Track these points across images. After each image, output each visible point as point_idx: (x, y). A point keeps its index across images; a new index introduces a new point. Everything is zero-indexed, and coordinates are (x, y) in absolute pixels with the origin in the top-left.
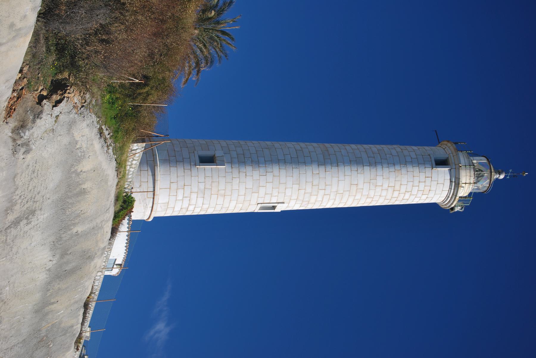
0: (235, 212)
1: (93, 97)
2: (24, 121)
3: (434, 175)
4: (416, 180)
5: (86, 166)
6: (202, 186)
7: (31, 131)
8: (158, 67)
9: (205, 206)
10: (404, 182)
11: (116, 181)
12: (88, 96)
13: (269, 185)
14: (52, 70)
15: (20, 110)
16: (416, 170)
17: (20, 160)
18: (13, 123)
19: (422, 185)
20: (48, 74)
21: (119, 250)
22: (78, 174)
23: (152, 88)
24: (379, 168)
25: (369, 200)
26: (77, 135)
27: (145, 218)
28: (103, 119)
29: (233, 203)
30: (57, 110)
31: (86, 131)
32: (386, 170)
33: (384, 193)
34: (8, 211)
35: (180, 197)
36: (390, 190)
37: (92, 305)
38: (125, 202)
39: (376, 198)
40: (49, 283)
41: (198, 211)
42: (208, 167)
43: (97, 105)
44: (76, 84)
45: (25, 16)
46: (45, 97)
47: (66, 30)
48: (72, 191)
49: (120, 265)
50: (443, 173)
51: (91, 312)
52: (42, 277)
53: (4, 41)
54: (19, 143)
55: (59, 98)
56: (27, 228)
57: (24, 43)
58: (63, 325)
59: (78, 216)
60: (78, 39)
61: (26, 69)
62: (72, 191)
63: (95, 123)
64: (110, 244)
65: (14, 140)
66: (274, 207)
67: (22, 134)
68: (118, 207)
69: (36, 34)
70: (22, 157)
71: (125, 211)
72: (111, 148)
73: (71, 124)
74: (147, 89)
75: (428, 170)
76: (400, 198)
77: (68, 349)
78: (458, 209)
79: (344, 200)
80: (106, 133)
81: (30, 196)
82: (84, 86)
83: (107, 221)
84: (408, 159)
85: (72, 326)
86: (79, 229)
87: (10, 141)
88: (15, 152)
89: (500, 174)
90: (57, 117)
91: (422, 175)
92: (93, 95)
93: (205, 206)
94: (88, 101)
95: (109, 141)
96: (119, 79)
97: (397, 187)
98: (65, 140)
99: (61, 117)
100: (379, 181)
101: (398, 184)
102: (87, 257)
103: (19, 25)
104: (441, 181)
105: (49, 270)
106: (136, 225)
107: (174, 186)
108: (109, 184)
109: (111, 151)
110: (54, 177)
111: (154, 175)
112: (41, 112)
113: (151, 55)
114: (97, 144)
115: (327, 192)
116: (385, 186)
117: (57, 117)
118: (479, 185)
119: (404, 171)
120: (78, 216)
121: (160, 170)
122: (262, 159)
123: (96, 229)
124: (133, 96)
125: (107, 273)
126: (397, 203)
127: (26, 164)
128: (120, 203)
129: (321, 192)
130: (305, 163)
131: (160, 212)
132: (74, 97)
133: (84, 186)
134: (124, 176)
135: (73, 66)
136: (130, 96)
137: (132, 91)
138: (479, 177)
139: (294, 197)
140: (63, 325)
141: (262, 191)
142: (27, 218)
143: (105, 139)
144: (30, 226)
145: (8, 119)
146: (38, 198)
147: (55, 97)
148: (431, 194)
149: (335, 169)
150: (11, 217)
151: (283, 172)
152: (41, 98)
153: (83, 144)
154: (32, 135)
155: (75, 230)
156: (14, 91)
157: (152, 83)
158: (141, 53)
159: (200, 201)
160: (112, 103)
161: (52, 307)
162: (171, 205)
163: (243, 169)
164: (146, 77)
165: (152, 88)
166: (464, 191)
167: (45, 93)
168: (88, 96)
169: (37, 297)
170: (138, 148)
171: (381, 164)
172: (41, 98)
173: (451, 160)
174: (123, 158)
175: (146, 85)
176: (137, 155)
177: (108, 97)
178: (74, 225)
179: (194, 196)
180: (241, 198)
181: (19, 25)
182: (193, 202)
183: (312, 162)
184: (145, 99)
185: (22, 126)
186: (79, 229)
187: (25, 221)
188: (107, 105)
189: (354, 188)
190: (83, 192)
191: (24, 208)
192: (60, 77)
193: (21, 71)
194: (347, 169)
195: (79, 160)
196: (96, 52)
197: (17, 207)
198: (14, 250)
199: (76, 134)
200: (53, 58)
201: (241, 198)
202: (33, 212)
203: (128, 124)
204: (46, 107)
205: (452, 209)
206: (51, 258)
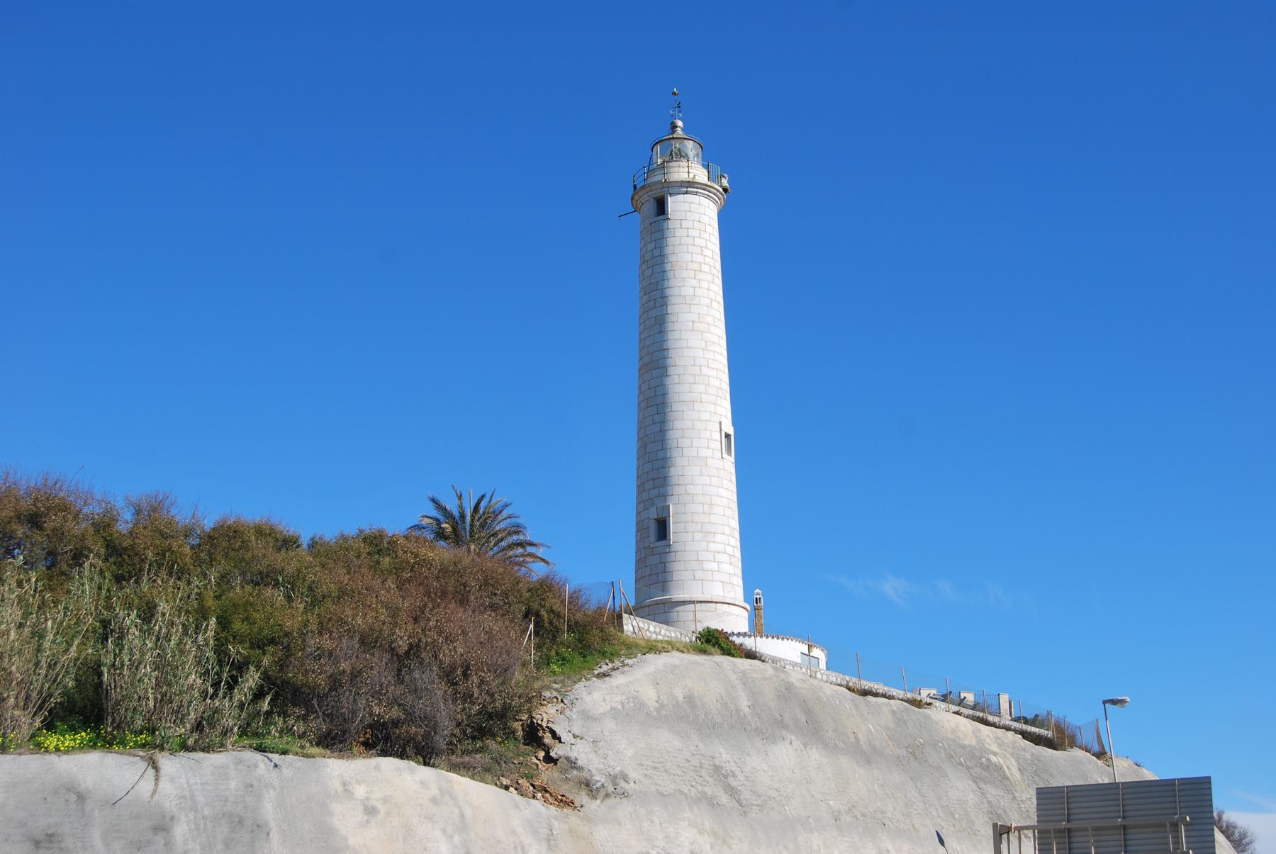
0: (735, 490)
1: (252, 646)
2: (580, 783)
3: (678, 216)
4: (684, 240)
5: (649, 695)
6: (698, 536)
7: (594, 772)
8: (511, 598)
9: (727, 530)
10: (688, 257)
11: (676, 653)
12: (547, 694)
13: (696, 443)
14: (511, 745)
15: (565, 789)
16: (671, 241)
17: (636, 787)
18: (582, 798)
19: (692, 233)
20: (511, 750)
21: (788, 650)
22: (662, 706)
23: (543, 606)
24: (668, 292)
25: (715, 305)
26: (603, 708)
27: (746, 614)
28: (585, 672)
29: (723, 492)
30: (565, 737)
31: (597, 695)
32: (672, 283)
33: (705, 284)
34: (713, 804)
35: (714, 566)
36: (700, 276)
37: (866, 685)
38: (708, 641)
39: (712, 295)
40: (826, 745)
41: (735, 541)
42: (672, 528)
43: (563, 682)
44: (530, 712)
45: (422, 783)
46: (547, 753)
47: (446, 726)
48: (686, 715)
49: (810, 647)
50: (673, 203)
51: (880, 688)
52: (815, 755)
53: (457, 811)
54: (611, 789)
55: (548, 735)
56: (741, 777)
57: (462, 783)
58: (891, 725)
59: (725, 705)
60: (464, 709)
61: (505, 781)
62: (686, 715)
63: (587, 683)
64: (774, 660)
65: (607, 795)
66: (727, 436)
67: (599, 785)
68: (716, 649)
69: (454, 768)
70: (632, 784)
71: (722, 641)
72: (627, 661)
73: (587, 716)
74: (543, 612)
75: (671, 224)
76: (711, 262)
77: (927, 717)
78: (725, 182)
79: (715, 339)
80: (605, 668)
81: (693, 774)
82: (533, 699)
83: (734, 665)
84: (656, 252)
85: (893, 712)
86: (744, 703)
87: (608, 802)
88: (624, 795)
89: (674, 127)
90: (575, 736)
91: (679, 232)
92: (548, 688)
93: (727, 530)
94: (555, 694)
95: (617, 663)
96: (528, 651)
97: (696, 267)
98: (609, 724)
99: (576, 731)
100: (687, 291)
101: (691, 266)
102: (787, 692)
103: (434, 791)
104: (686, 207)
105: (805, 745)
106: (757, 629)
107: (699, 575)
108: (678, 662)
109: (630, 662)
110: (665, 740)
111: (684, 603)
112: (567, 758)
113: (493, 607)
114: (618, 680)
115: (704, 362)
116: (694, 282)
117: (575, 736)
118: (691, 154)
119: (672, 258)
120: (725, 705)
121: (677, 595)
122: (660, 454)
123: (744, 678)
124: (555, 633)
125: (823, 665)
126: (718, 266)
127: (642, 779)
128: (709, 647)
129: (705, 370)
130: (664, 395)
131: (737, 594)
132: (547, 714)
133: (680, 697)
134: (669, 643)
135: (503, 715)
136: (554, 636)
137: (546, 632)
138: (681, 155)
139: (711, 408)
140: (891, 725)
141: (704, 453)
142: (726, 777)
143: (614, 669)
144: (738, 773)
145: (577, 804)
146: (695, 762)
147: (548, 739)
148: (705, 219)
149: (672, 353)
150: (724, 799)
151: (677, 424)
152: (549, 759)
153: (616, 700)
154: (599, 771)
155: (747, 710)
156: (534, 797)
157: (535, 606)
158: (488, 620)
159: (719, 538)
160: (563, 660)
161: (862, 739)
162: (726, 578)
163: (674, 480)
164: (526, 615)
165: (543, 606)
166: (701, 175)
167: (542, 754)
168: (547, 694)
169: (844, 760)
170: (631, 625)
171: (663, 289)
172: (549, 759)
173: (657, 193)
174: (642, 643)
175: (537, 615)
176: (641, 625)
177: (554, 667)
178: (738, 711)
179: (712, 547)
180: (714, 481)
181: (434, 791)
182: (720, 547)
183: (663, 385)
184: (559, 615)
185: (587, 785)
186: (744, 703)
187: (731, 780)
188: (566, 669)
189: (697, 326)
190: (690, 699)
191: (711, 780)
192: (520, 733)
193: (507, 788)
194: (670, 336)
195: (640, 705)
196: (482, 682)
197: (709, 791)
198: (773, 794)
199: (601, 710)
200: (492, 744)
201: (714, 481)
202: (717, 769)
203: (594, 638)
204: (560, 753)
205: (725, 190)
206: (787, 742)
